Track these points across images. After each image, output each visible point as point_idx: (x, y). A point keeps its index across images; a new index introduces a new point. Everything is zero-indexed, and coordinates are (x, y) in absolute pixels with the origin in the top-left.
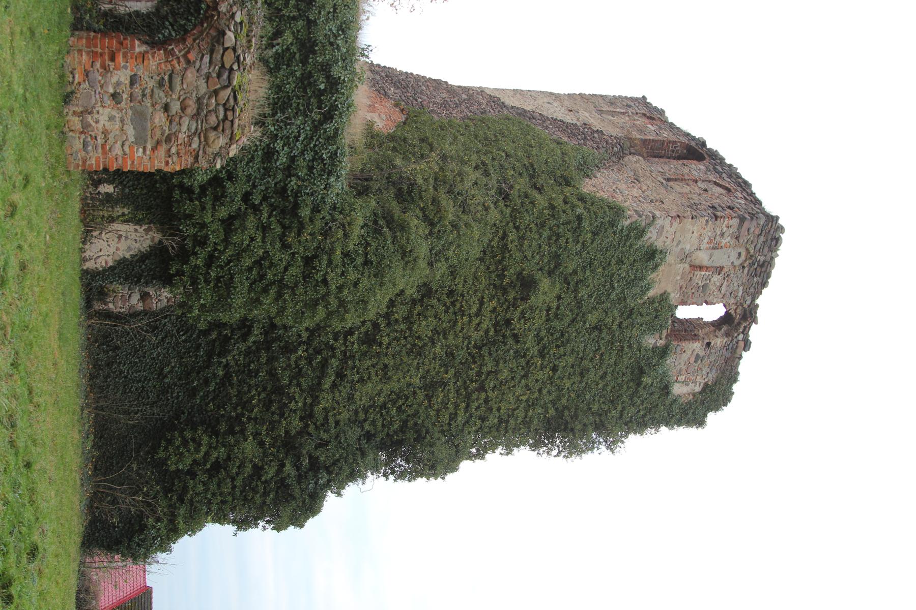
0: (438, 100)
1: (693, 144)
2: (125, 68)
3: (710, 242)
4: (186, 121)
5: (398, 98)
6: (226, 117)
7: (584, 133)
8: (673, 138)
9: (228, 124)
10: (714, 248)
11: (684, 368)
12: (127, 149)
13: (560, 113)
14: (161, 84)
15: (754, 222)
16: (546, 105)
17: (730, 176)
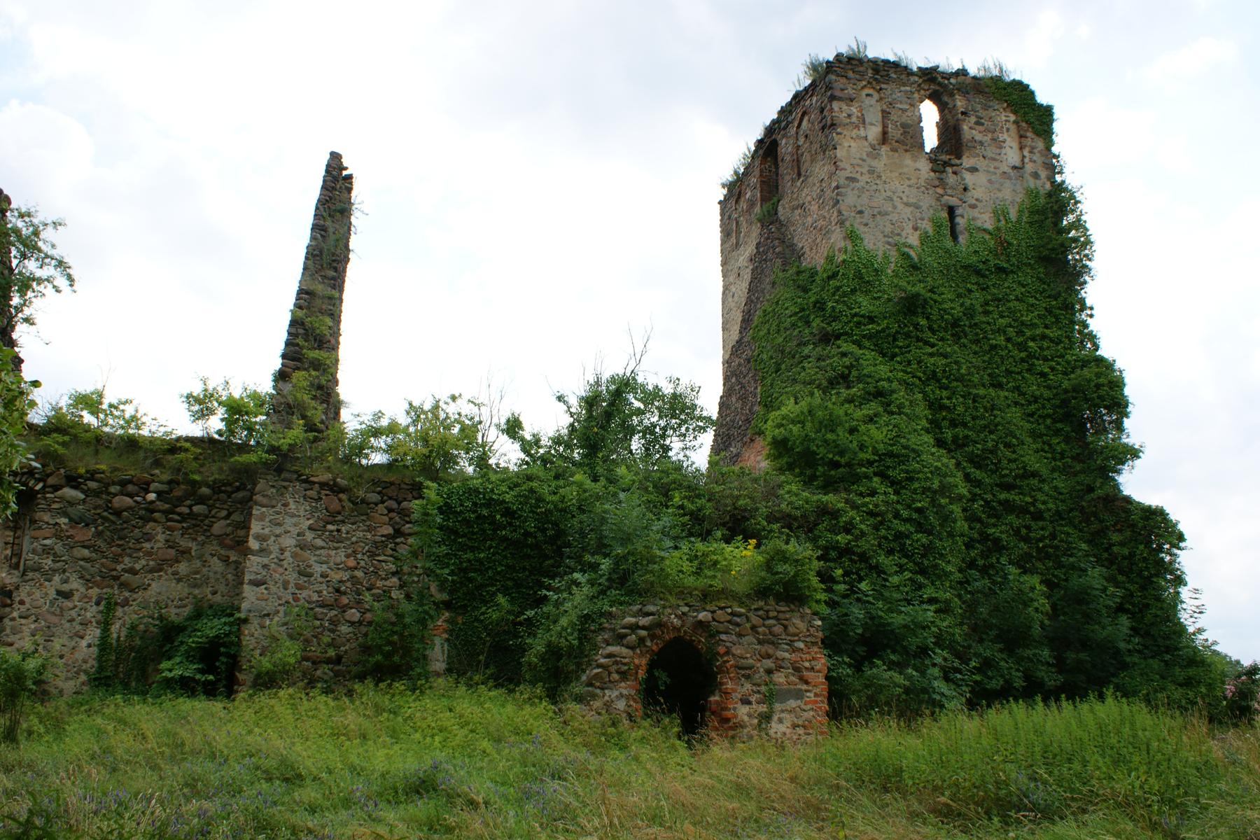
0: (739, 405)
1: (761, 152)
2: (735, 709)
3: (857, 127)
4: (780, 654)
5: (740, 444)
6: (775, 618)
7: (760, 260)
8: (757, 173)
9: (781, 616)
10: (864, 122)
11: (990, 135)
12: (809, 707)
13: (742, 288)
14: (748, 677)
15: (835, 85)
16: (736, 298)
17: (790, 112)
